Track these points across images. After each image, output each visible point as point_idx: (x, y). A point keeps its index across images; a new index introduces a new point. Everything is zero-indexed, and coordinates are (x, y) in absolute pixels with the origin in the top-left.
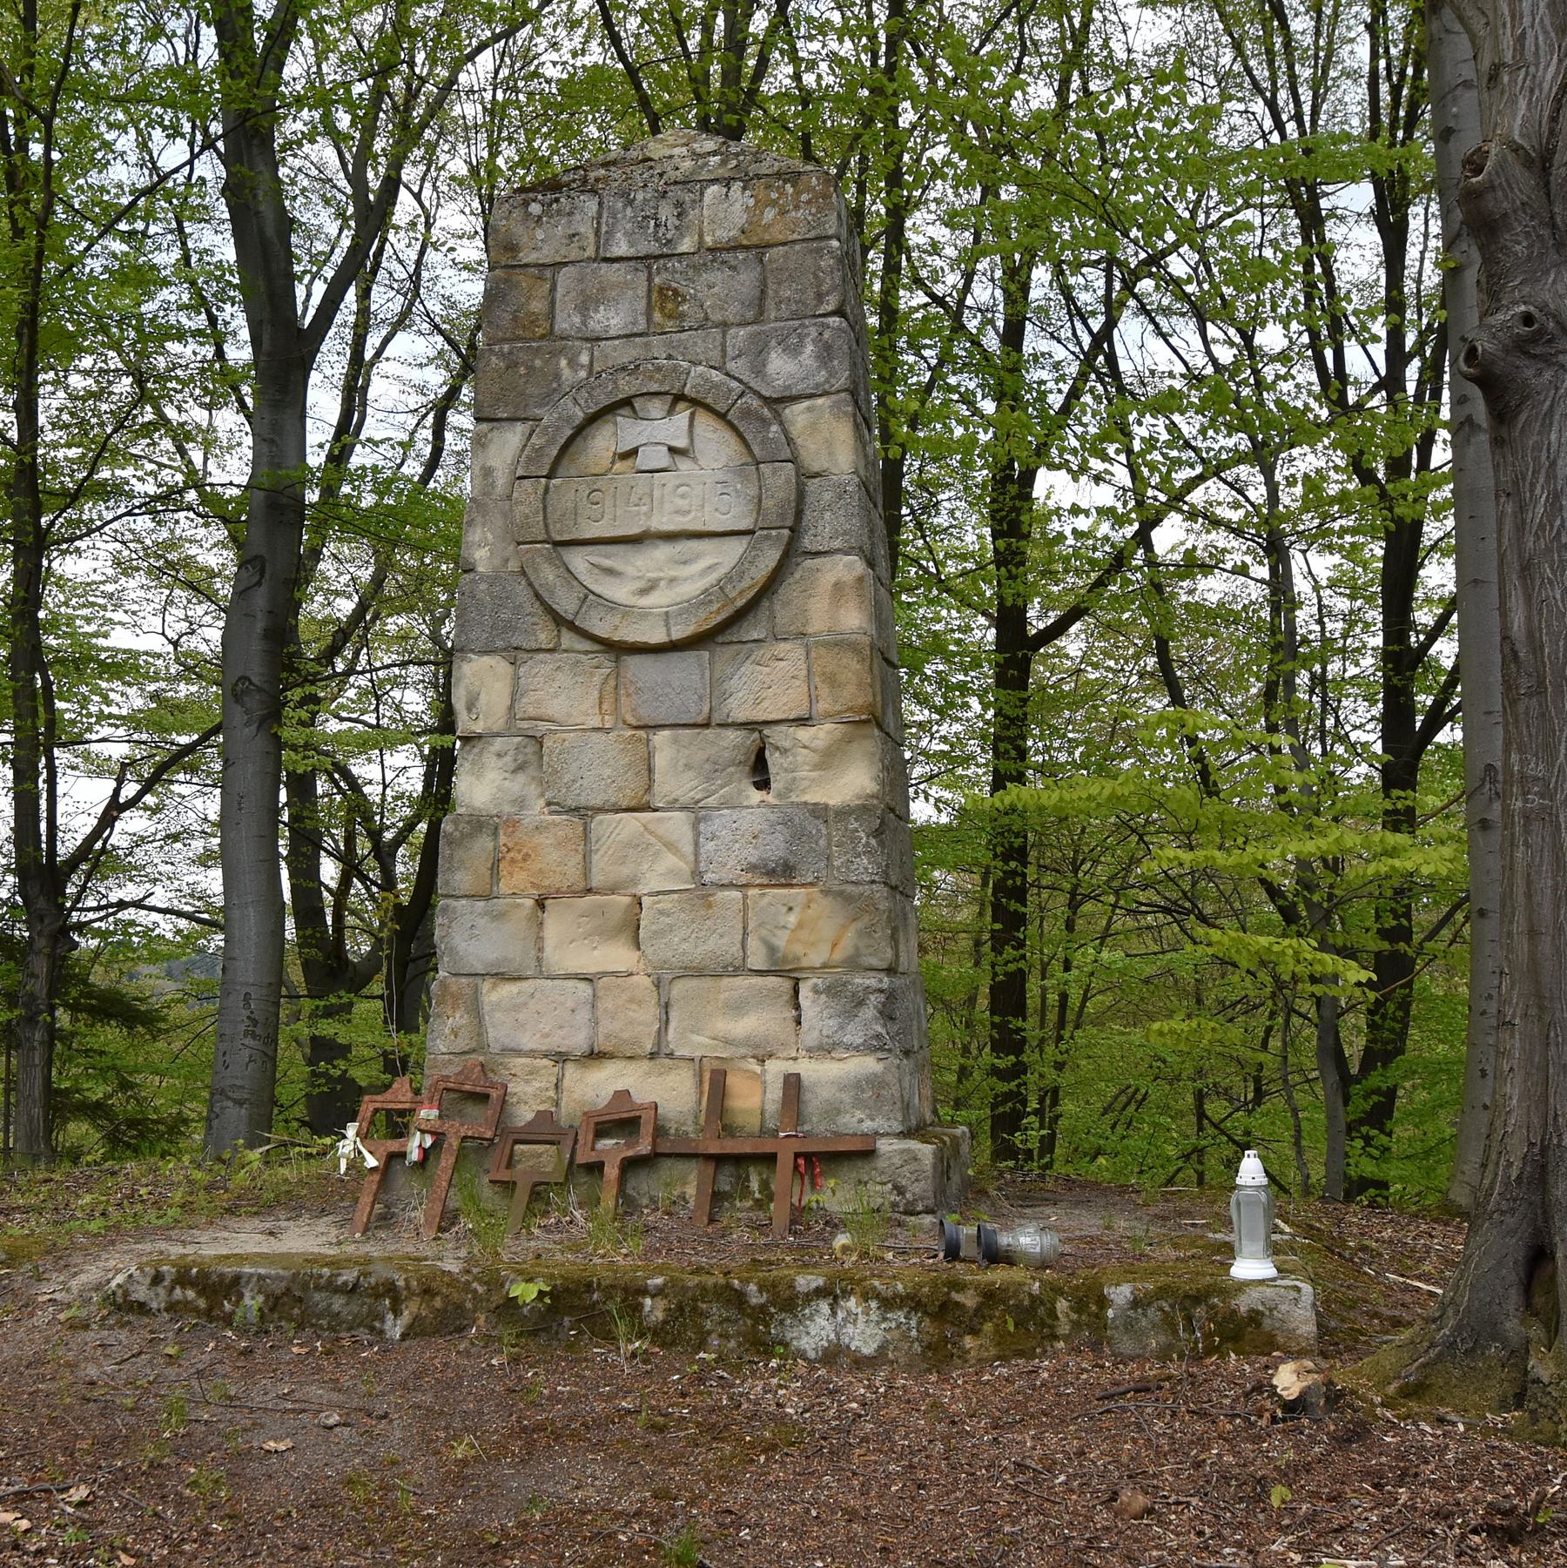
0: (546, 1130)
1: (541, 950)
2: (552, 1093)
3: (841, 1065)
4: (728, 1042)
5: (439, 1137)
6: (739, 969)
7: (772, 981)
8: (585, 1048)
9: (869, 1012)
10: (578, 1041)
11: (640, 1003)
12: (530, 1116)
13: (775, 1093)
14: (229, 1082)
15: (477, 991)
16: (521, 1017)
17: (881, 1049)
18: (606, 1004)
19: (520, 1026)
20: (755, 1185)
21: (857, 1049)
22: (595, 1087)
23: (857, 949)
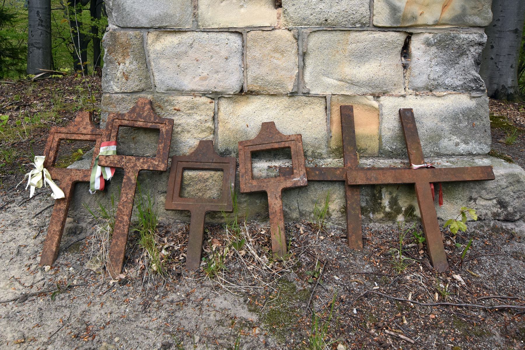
0: (211, 156)
1: (196, 7)
2: (210, 124)
3: (440, 101)
4: (353, 83)
5: (119, 173)
6: (366, 25)
7: (392, 35)
8: (237, 88)
9: (468, 61)
10: (231, 82)
11: (282, 53)
12: (196, 143)
13: (391, 124)
14: (34, 41)
15: (143, 42)
16: (182, 63)
17: (477, 90)
18: (254, 52)
19: (181, 70)
20: (386, 202)
21: (455, 89)
22: (245, 119)
23: (464, 9)
